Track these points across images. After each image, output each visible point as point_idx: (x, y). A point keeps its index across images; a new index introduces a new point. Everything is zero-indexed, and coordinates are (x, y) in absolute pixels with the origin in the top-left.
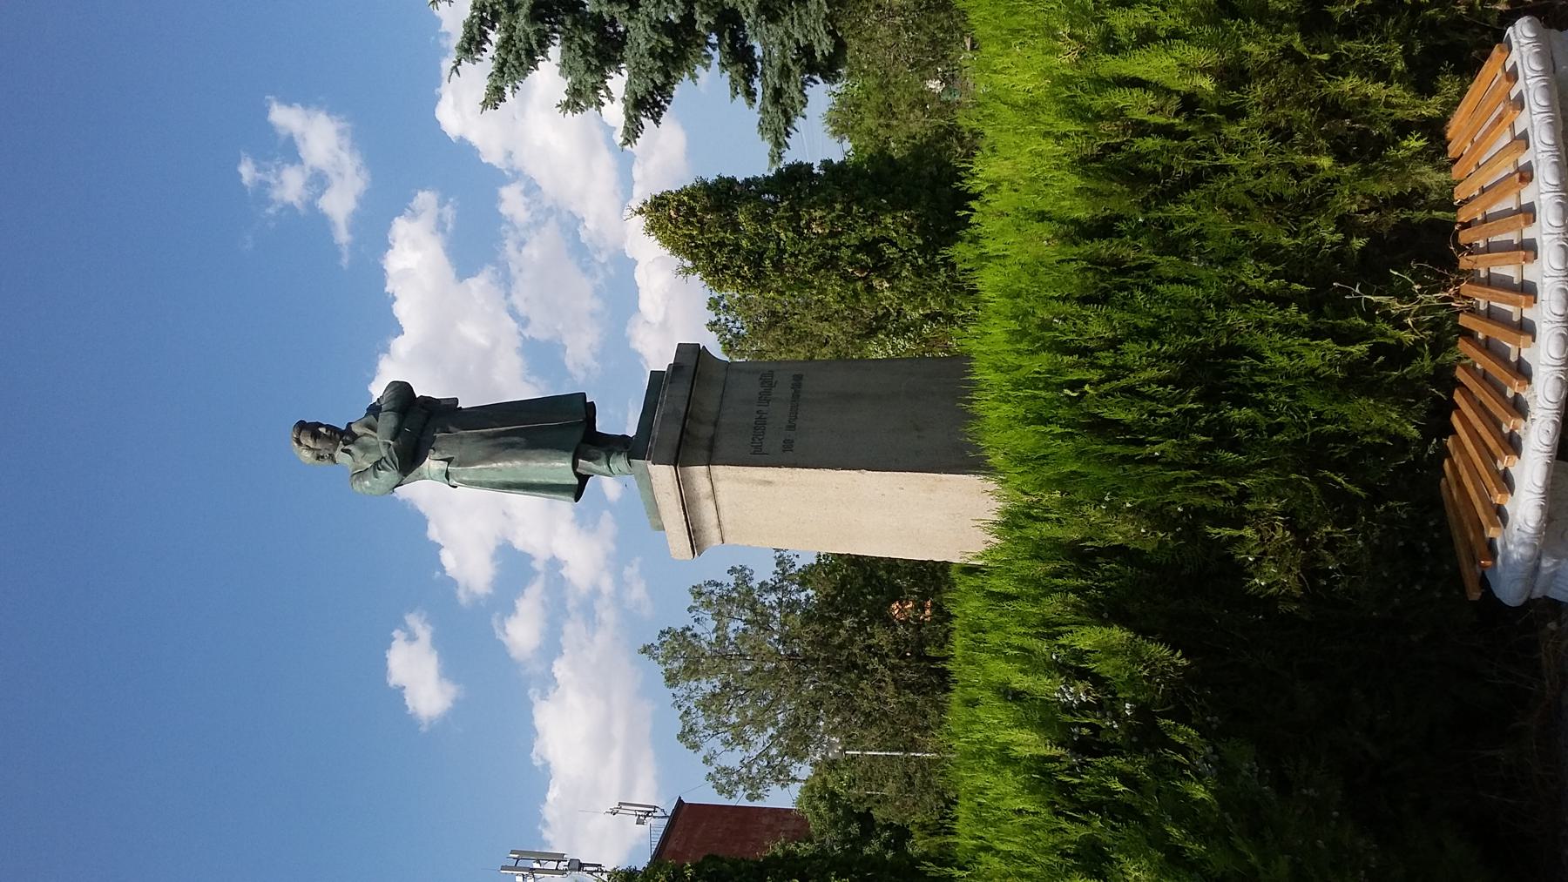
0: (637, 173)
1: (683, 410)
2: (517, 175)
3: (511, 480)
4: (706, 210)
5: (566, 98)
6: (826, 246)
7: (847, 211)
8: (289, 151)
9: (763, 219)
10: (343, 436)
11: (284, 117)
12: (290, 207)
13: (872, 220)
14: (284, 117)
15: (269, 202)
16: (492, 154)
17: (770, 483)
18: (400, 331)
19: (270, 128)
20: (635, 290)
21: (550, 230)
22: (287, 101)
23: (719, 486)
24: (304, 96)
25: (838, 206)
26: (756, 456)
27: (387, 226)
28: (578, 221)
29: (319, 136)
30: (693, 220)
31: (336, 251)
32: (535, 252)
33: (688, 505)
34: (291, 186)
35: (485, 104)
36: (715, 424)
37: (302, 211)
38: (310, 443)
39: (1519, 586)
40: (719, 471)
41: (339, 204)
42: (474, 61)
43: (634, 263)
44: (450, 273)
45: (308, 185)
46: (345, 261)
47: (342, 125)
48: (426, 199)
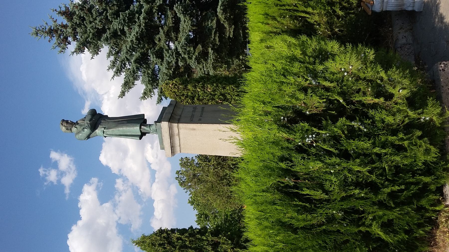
0: (156, 176)
1: (172, 112)
2: (121, 176)
3: (122, 134)
4: (179, 84)
5: (142, 95)
6: (211, 94)
7: (217, 86)
8: (55, 165)
9: (195, 87)
10: (73, 124)
11: (54, 155)
12: (52, 183)
13: (224, 88)
14: (54, 155)
15: (46, 181)
16: (115, 170)
17: (194, 129)
18: (80, 219)
19: (51, 159)
20: (153, 209)
21: (130, 192)
22: (56, 151)
23: (181, 131)
24: (62, 150)
25: (215, 84)
26: (192, 121)
27: (82, 187)
28: (138, 188)
29: (64, 161)
30: (176, 87)
31: (65, 195)
32: (125, 197)
33: (171, 137)
34: (53, 176)
35: (119, 97)
36: (180, 116)
37: (55, 183)
38: (65, 125)
39: (380, 5)
40: (181, 125)
41: (67, 181)
42: (118, 76)
43: (154, 201)
44: (98, 203)
45: (57, 175)
46: (67, 198)
47: (71, 159)
48: (95, 180)
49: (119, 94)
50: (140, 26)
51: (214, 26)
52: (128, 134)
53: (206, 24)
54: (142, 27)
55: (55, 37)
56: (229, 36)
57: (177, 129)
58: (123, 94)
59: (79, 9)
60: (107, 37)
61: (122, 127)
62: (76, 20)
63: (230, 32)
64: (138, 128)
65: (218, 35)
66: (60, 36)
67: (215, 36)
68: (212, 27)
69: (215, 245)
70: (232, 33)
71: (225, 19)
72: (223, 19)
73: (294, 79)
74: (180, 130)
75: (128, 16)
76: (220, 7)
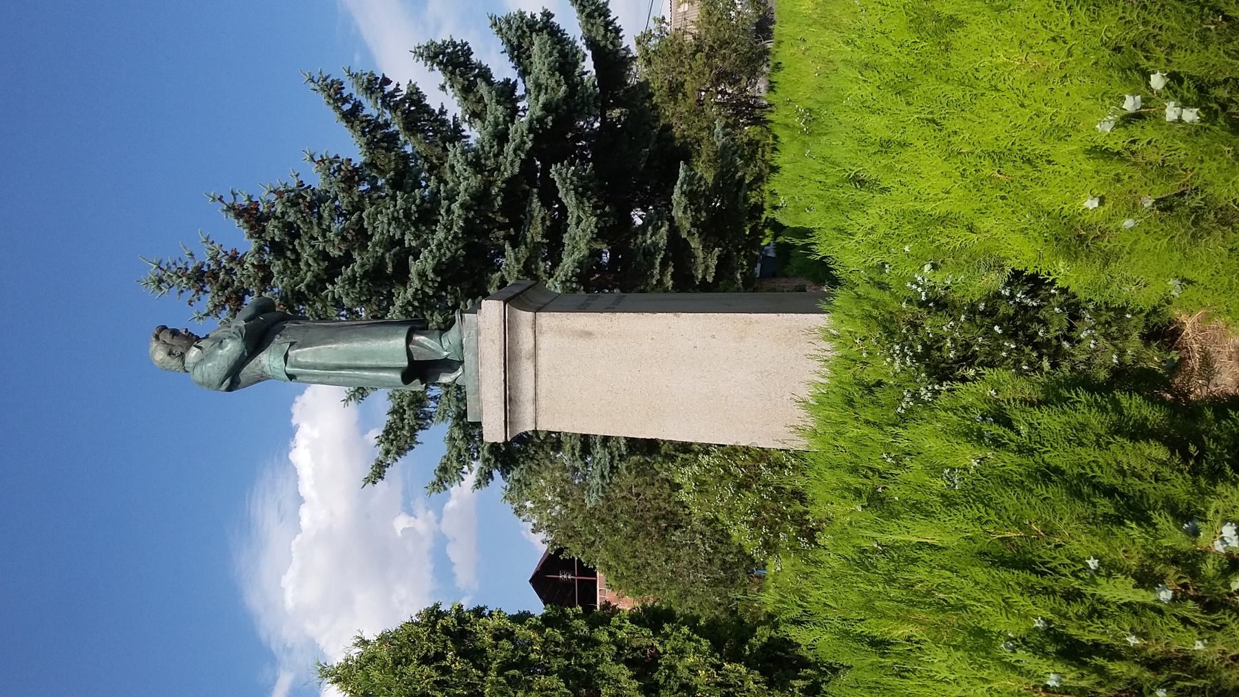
23: (544, 342)
33: (510, 359)
35: (367, 480)
49: (368, 472)
50: (448, 229)
51: (662, 243)
52: (366, 363)
53: (640, 240)
54: (455, 229)
55: (209, 296)
56: (704, 278)
57: (530, 332)
58: (379, 471)
59: (284, 199)
60: (354, 275)
61: (349, 339)
62: (272, 229)
63: (707, 267)
64: (400, 342)
65: (671, 269)
66: (223, 288)
67: (662, 273)
68: (655, 244)
69: (643, 665)
70: (712, 270)
71: (693, 225)
72: (688, 226)
73: (908, 330)
74: (540, 338)
75: (418, 201)
76: (682, 184)
